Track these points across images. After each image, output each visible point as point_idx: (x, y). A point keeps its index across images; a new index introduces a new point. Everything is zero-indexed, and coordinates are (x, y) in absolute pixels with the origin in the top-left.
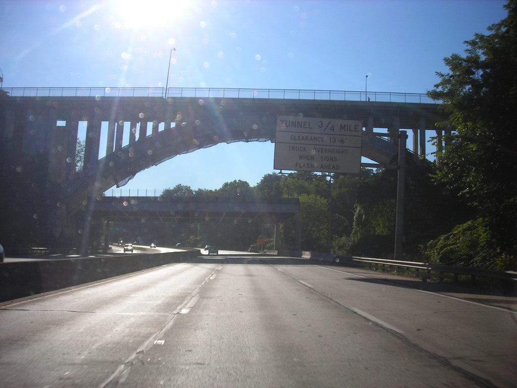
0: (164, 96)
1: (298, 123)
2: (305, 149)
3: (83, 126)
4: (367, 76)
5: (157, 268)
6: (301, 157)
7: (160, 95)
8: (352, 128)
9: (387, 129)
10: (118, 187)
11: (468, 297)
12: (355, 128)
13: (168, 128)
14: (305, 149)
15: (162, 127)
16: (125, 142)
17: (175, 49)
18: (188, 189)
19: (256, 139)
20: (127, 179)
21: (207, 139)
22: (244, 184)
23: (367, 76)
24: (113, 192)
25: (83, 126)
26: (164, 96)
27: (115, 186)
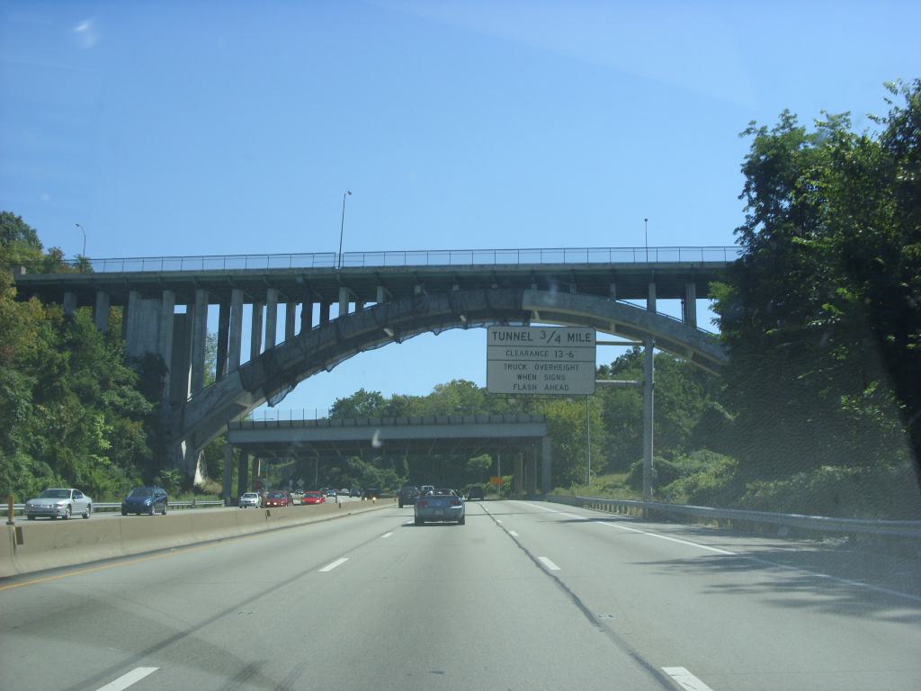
0: (337, 265)
1: (507, 334)
2: (524, 366)
3: (214, 311)
4: (646, 220)
5: (323, 268)
6: (520, 377)
7: (331, 265)
8: (583, 338)
9: (680, 300)
10: (270, 405)
11: (770, 543)
12: (587, 337)
13: (344, 316)
14: (524, 366)
15: (334, 311)
16: (280, 338)
17: (350, 193)
18: (376, 397)
19: (479, 324)
20: (284, 392)
21: (404, 328)
22: (463, 387)
23: (646, 220)
24: (261, 412)
25: (214, 311)
26: (337, 265)
27: (267, 403)
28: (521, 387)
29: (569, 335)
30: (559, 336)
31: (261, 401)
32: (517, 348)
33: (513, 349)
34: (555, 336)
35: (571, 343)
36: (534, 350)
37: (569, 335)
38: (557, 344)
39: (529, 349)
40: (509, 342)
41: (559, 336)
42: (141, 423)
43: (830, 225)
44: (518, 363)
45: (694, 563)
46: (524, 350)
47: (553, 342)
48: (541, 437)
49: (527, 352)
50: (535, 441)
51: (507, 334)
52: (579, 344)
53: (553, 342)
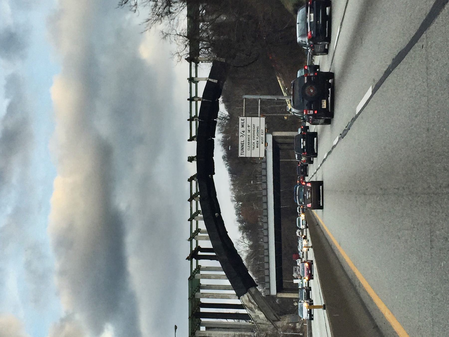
1: (241, 149)
2: (254, 143)
8: (243, 121)
12: (243, 120)
28: (258, 136)
29: (242, 127)
30: (242, 131)
31: (203, 323)
32: (247, 146)
33: (247, 148)
34: (242, 133)
35: (245, 126)
36: (247, 140)
37: (242, 127)
38: (245, 132)
39: (247, 142)
40: (245, 149)
41: (242, 131)
42: (186, 4)
43: (254, 204)
44: (252, 145)
45: (224, 328)
46: (247, 148)
47: (245, 134)
48: (273, 136)
49: (249, 143)
50: (274, 138)
51: (241, 149)
52: (245, 123)
53: (245, 134)
